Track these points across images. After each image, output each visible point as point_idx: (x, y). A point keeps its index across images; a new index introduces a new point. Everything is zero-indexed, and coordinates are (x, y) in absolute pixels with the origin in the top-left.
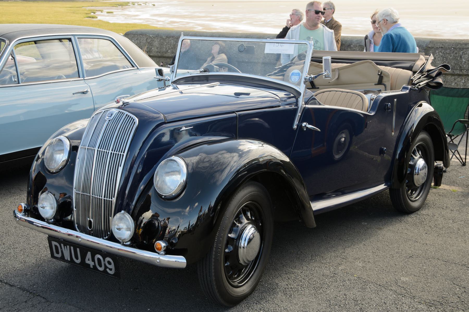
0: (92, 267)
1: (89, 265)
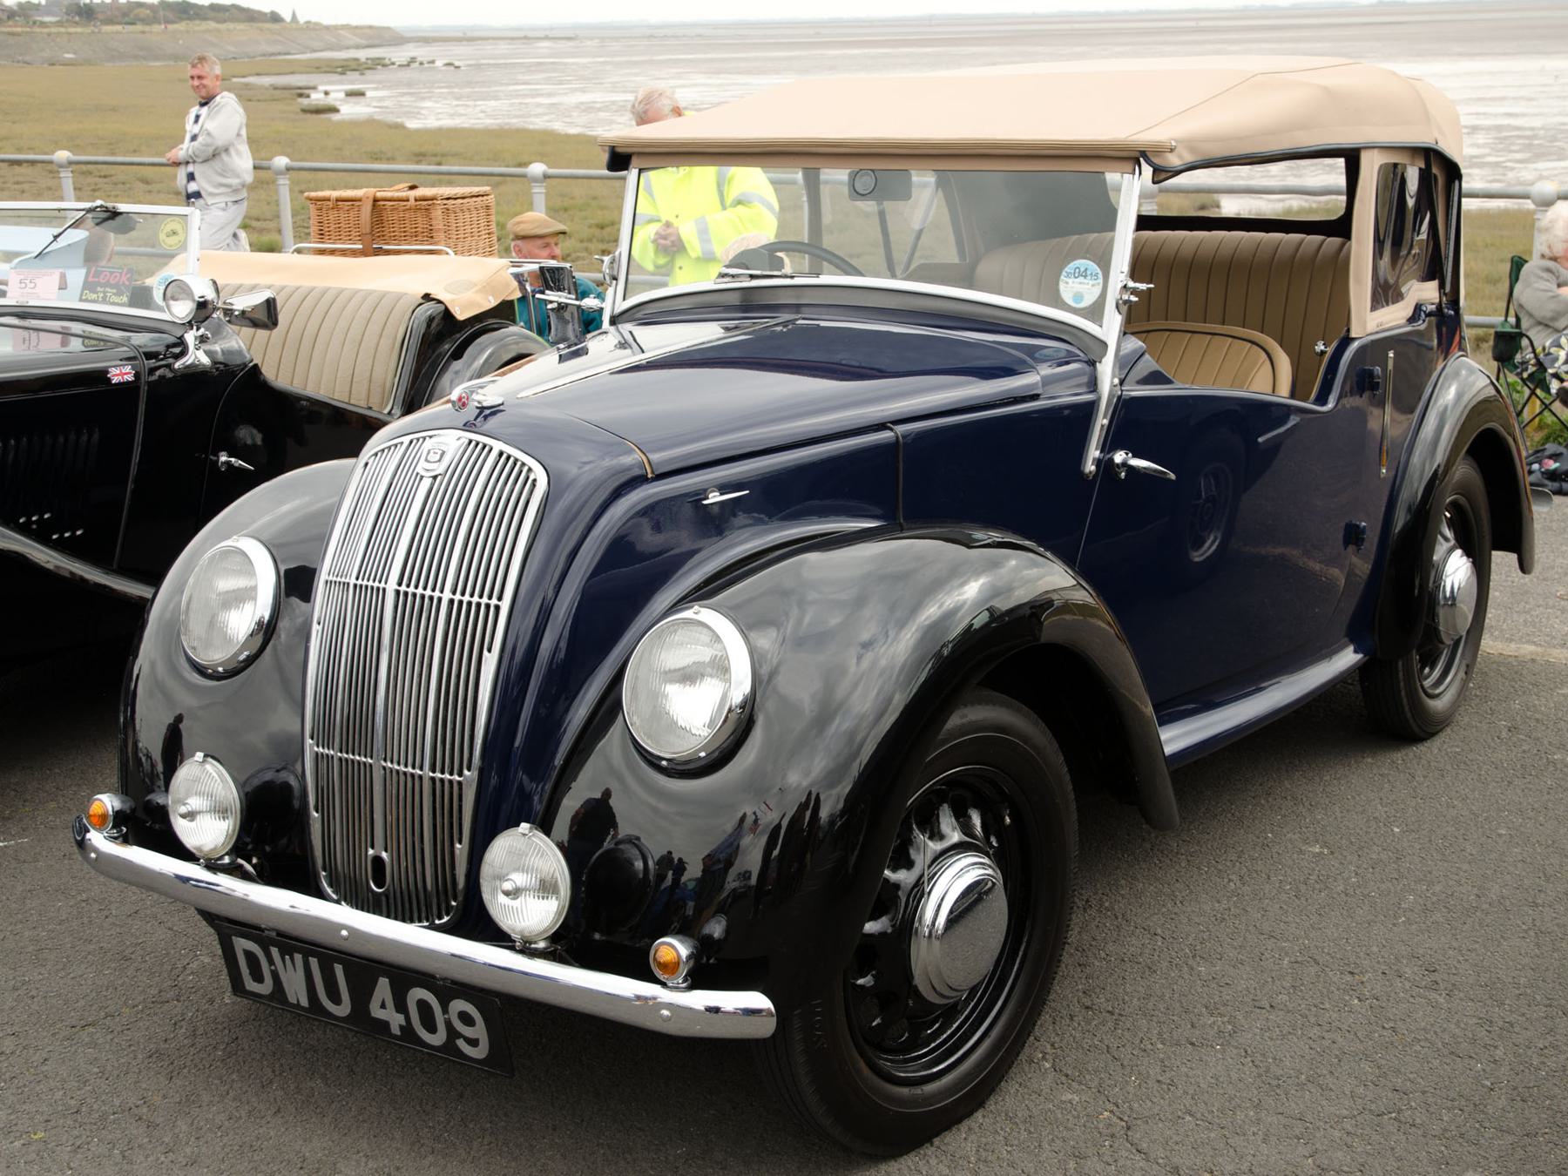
0: (396, 1031)
1: (385, 1025)
